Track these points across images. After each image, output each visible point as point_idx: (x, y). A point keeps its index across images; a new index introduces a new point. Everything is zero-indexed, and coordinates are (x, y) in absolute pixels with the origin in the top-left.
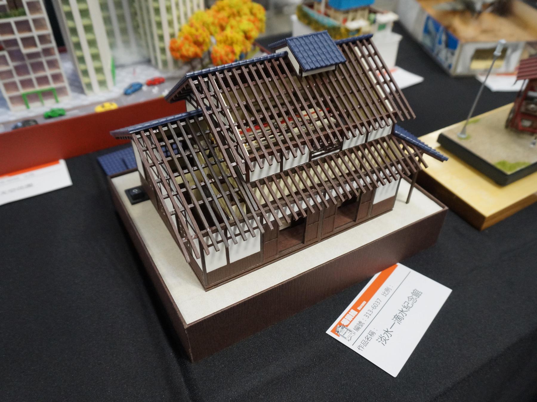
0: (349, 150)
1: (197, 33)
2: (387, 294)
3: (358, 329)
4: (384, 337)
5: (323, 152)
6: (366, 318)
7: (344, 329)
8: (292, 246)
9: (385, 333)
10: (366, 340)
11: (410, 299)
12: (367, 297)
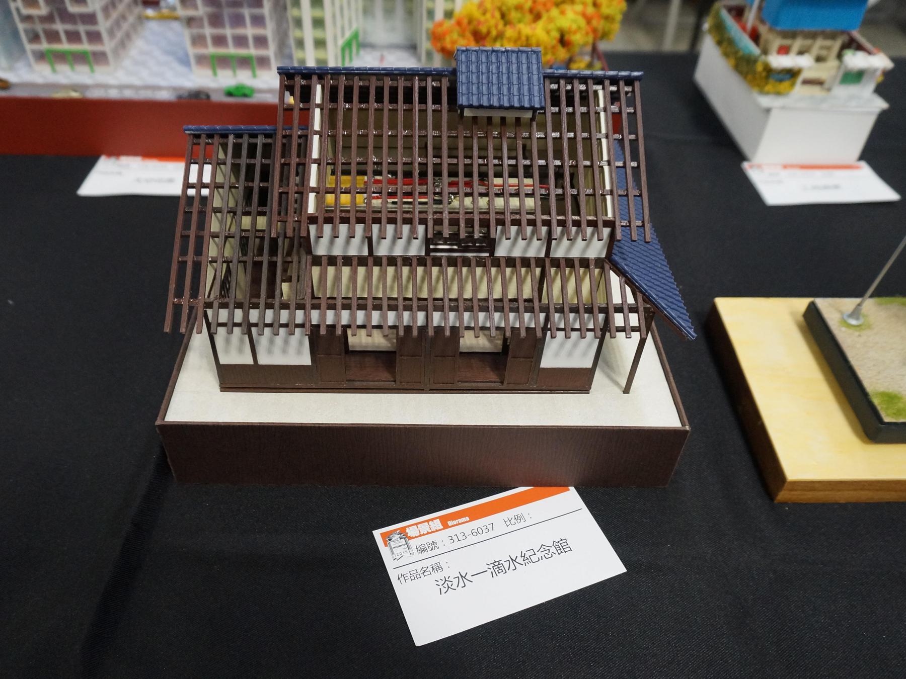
0: (508, 259)
1: (482, 19)
2: (513, 523)
3: (422, 550)
4: (452, 582)
5: (455, 247)
6: (449, 541)
7: (403, 540)
8: (376, 379)
9: (458, 577)
10: (420, 573)
11: (542, 550)
12: (474, 515)
